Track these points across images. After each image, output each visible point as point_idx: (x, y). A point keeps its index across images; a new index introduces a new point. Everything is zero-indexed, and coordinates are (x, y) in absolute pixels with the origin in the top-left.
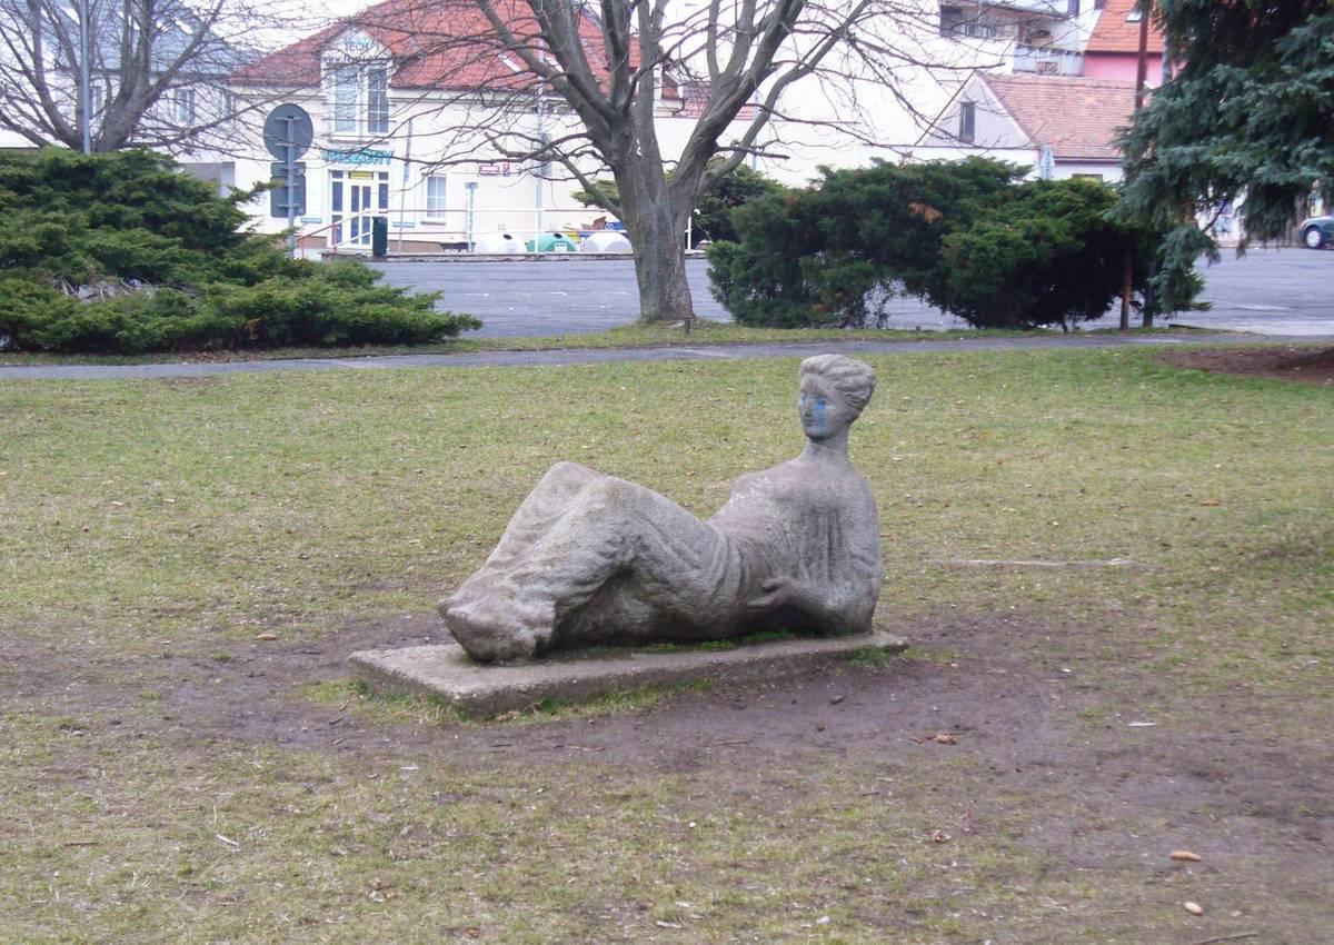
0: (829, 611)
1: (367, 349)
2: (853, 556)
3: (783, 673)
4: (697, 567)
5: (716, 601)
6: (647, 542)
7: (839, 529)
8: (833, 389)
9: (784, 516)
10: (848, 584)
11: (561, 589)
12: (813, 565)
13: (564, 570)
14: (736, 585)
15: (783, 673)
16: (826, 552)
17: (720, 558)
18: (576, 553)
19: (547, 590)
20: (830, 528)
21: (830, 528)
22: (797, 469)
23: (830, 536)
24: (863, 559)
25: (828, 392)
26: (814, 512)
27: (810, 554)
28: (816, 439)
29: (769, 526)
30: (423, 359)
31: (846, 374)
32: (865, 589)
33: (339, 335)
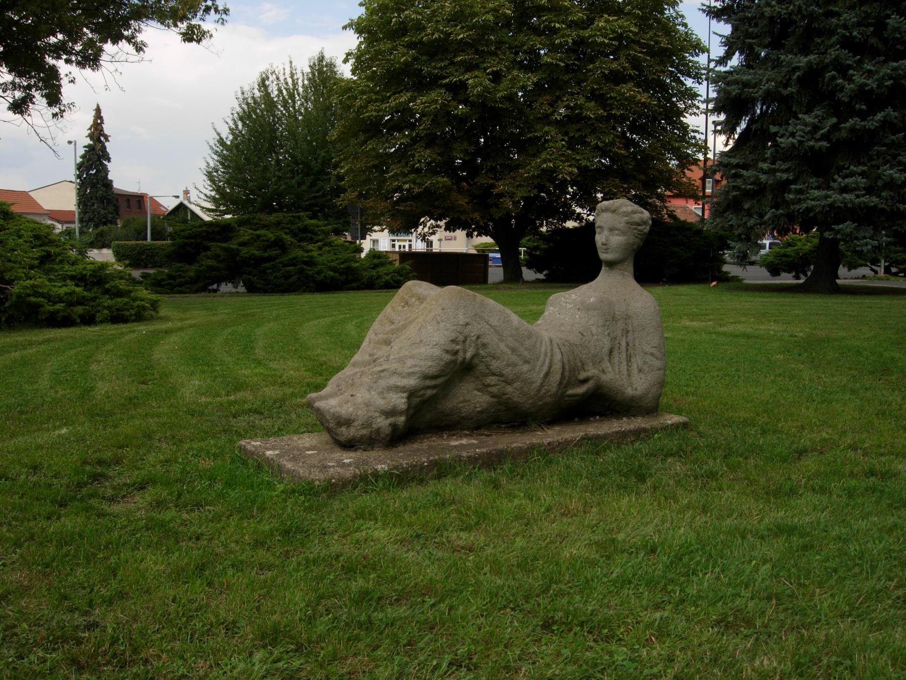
11: (412, 382)
17: (546, 355)
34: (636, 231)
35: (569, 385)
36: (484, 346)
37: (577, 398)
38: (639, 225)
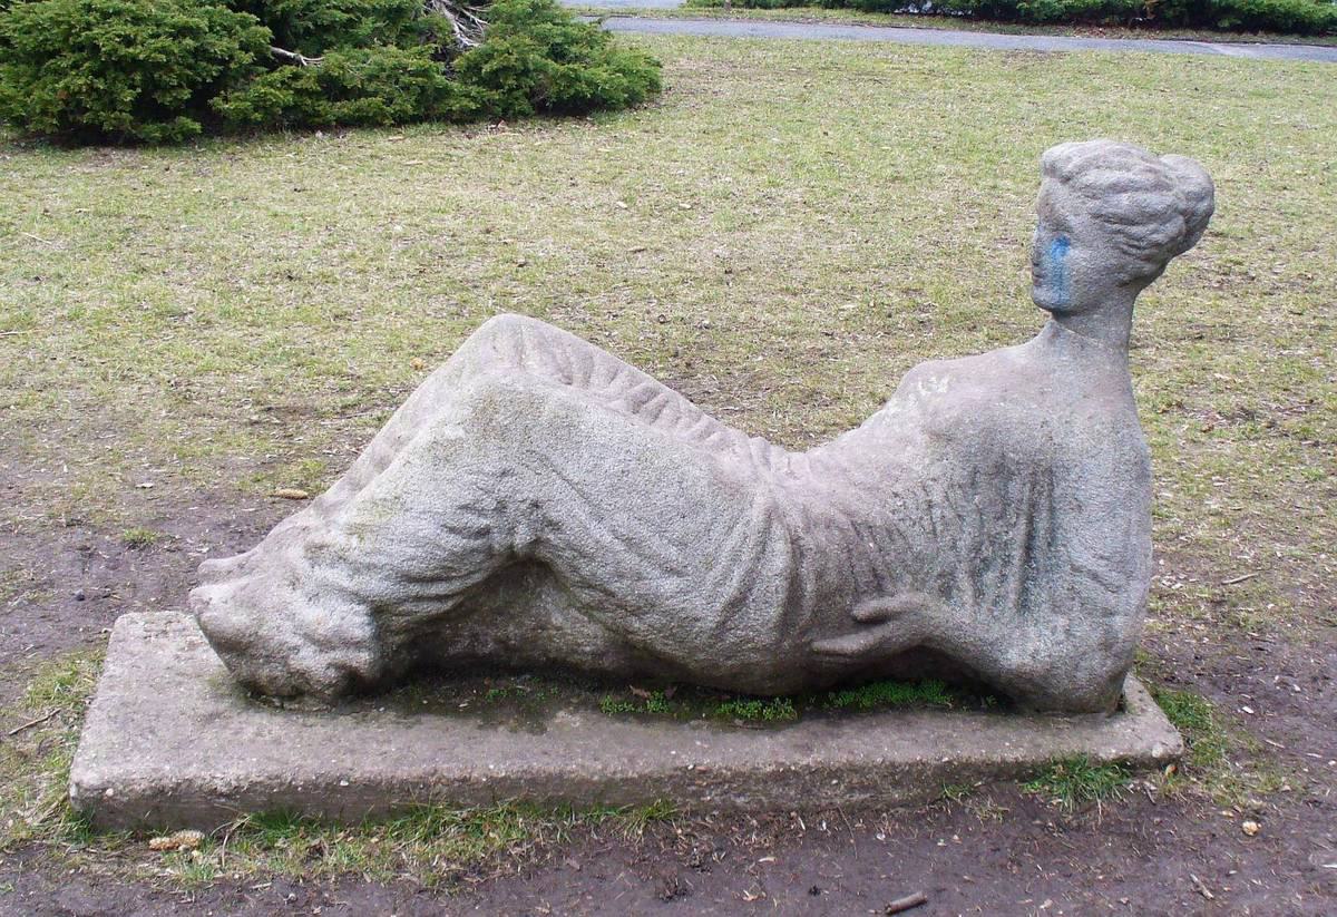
0: (1010, 671)
1: (1261, 36)
2: (1076, 569)
3: (858, 797)
4: (672, 572)
5: (730, 638)
6: (553, 515)
7: (1052, 510)
8: (1085, 218)
9: (936, 470)
10: (1061, 621)
11: (377, 586)
12: (990, 577)
13: (379, 552)
14: (774, 613)
15: (858, 797)
16: (1017, 554)
17: (735, 558)
18: (404, 524)
19: (346, 583)
20: (1033, 505)
21: (1033, 505)
22: (1011, 381)
23: (1031, 521)
24: (1095, 577)
25: (1073, 221)
26: (1001, 471)
27: (987, 552)
28: (1060, 313)
29: (899, 488)
30: (1312, 50)
31: (1117, 188)
32: (1096, 637)
33: (1234, 20)
34: (1121, 238)
35: (820, 623)
36: (555, 526)
37: (842, 660)
38: (1133, 223)
